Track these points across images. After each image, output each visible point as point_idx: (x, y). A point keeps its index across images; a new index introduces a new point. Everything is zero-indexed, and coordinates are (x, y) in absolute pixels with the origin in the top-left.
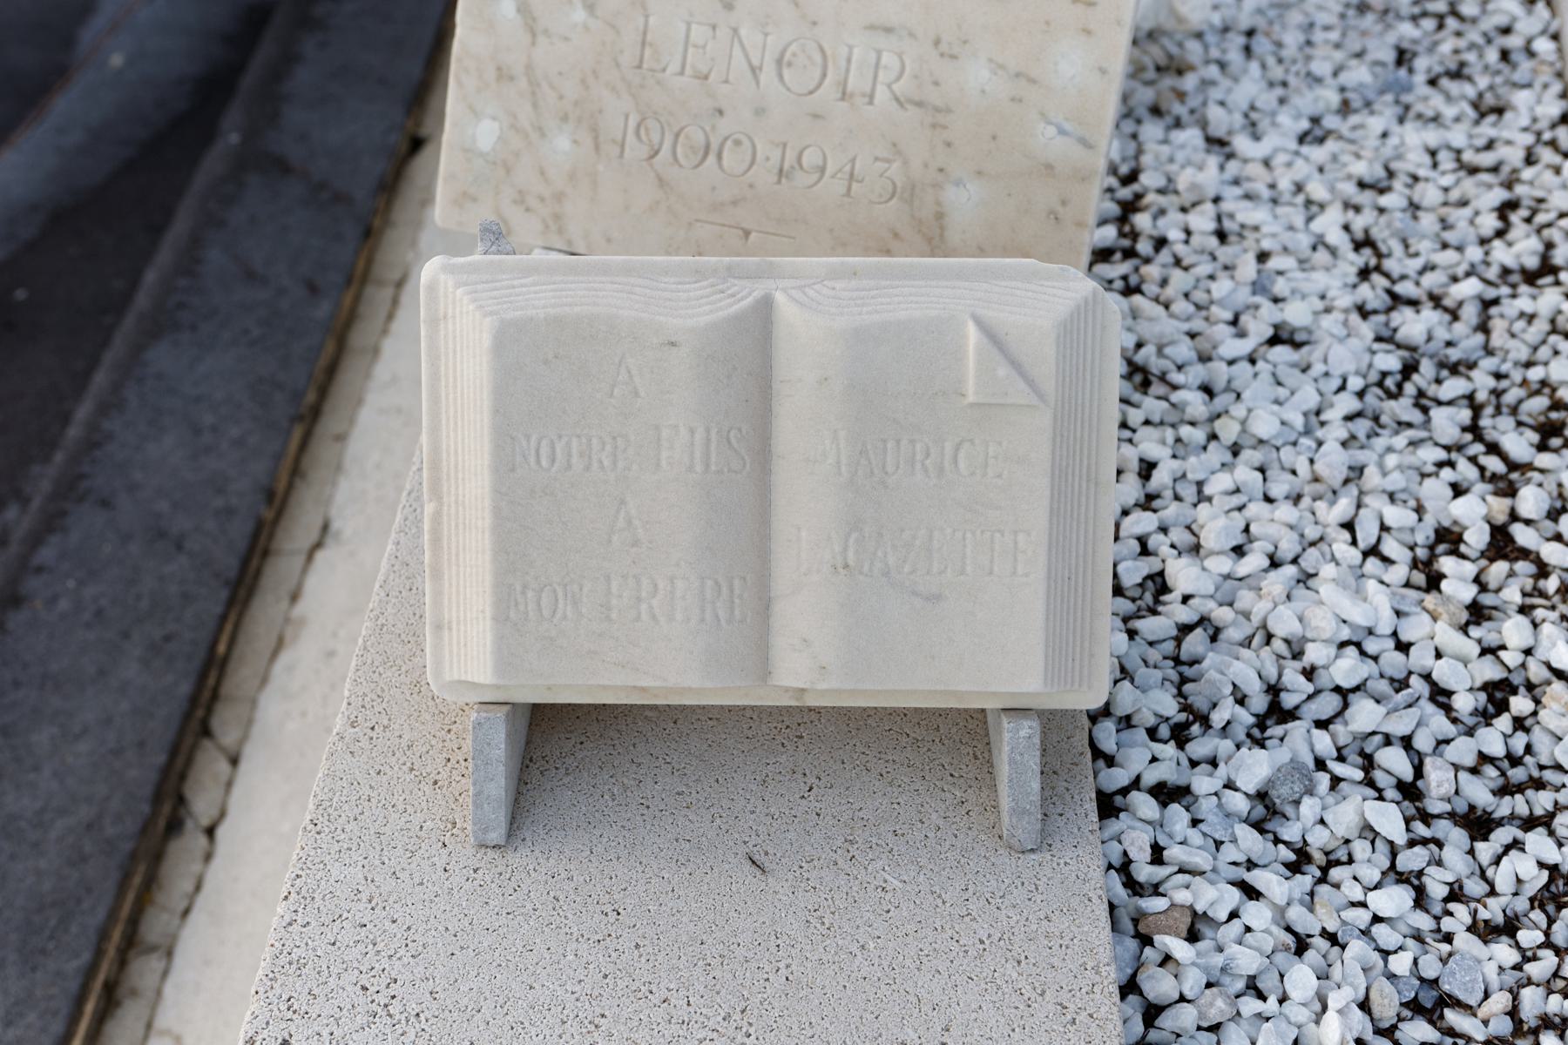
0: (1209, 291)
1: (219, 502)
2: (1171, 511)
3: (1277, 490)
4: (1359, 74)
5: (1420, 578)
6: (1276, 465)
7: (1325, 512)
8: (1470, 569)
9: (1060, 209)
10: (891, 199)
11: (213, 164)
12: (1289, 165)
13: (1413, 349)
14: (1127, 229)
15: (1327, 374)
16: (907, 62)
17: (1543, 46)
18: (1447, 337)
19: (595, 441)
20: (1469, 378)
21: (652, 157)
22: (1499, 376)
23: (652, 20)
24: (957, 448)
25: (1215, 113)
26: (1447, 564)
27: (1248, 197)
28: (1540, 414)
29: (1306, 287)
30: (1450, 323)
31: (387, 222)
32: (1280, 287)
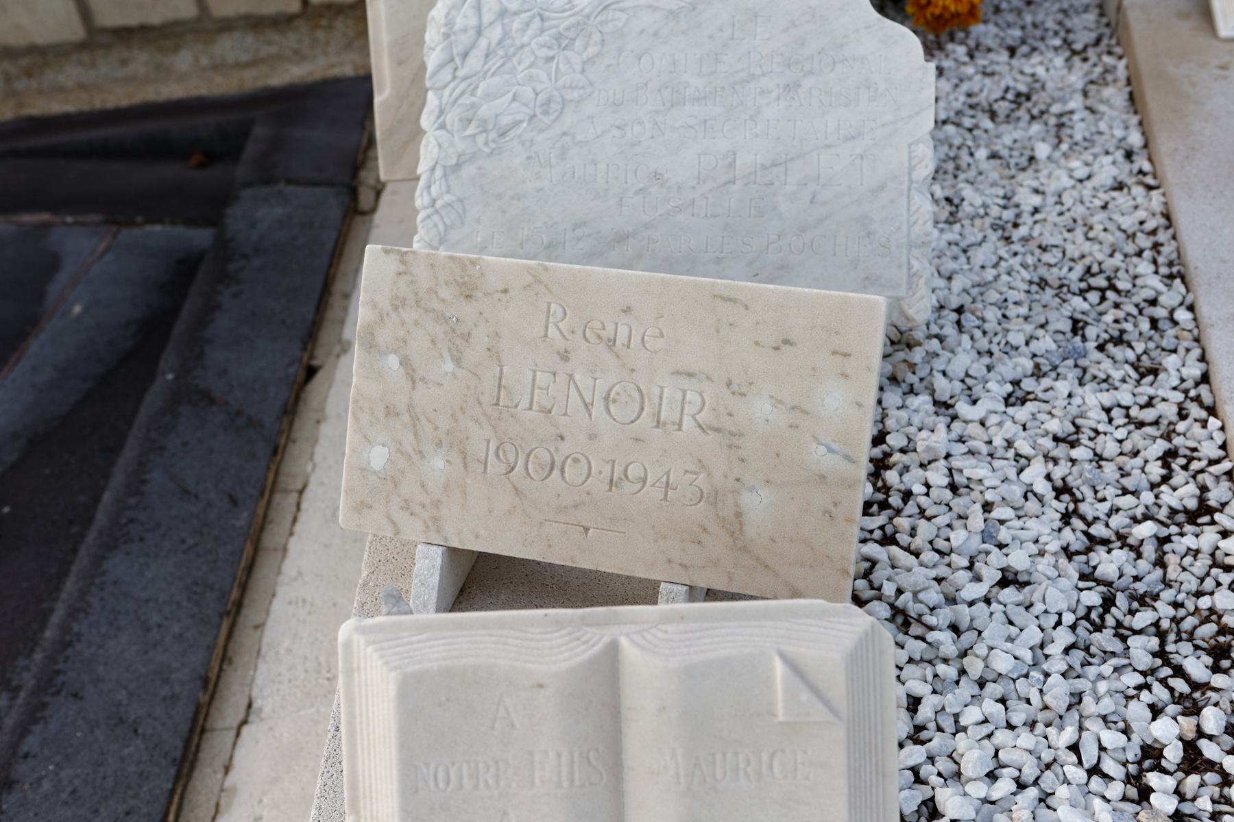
0: (948, 540)
1: (165, 691)
2: (938, 742)
3: (1017, 719)
4: (1045, 343)
5: (1133, 792)
6: (1014, 696)
7: (1055, 737)
8: (1170, 782)
9: (833, 509)
10: (699, 502)
11: (154, 398)
12: (1000, 424)
13: (1109, 584)
14: (880, 484)
15: (1046, 612)
16: (707, 399)
17: (1182, 315)
18: (1134, 573)
19: (481, 765)
20: (1155, 609)
21: (510, 472)
22: (1176, 605)
23: (505, 369)
24: (772, 757)
25: (940, 383)
26: (1153, 779)
27: (971, 452)
28: (1211, 638)
29: (1023, 535)
30: (1135, 560)
31: (290, 440)
32: (1004, 535)
